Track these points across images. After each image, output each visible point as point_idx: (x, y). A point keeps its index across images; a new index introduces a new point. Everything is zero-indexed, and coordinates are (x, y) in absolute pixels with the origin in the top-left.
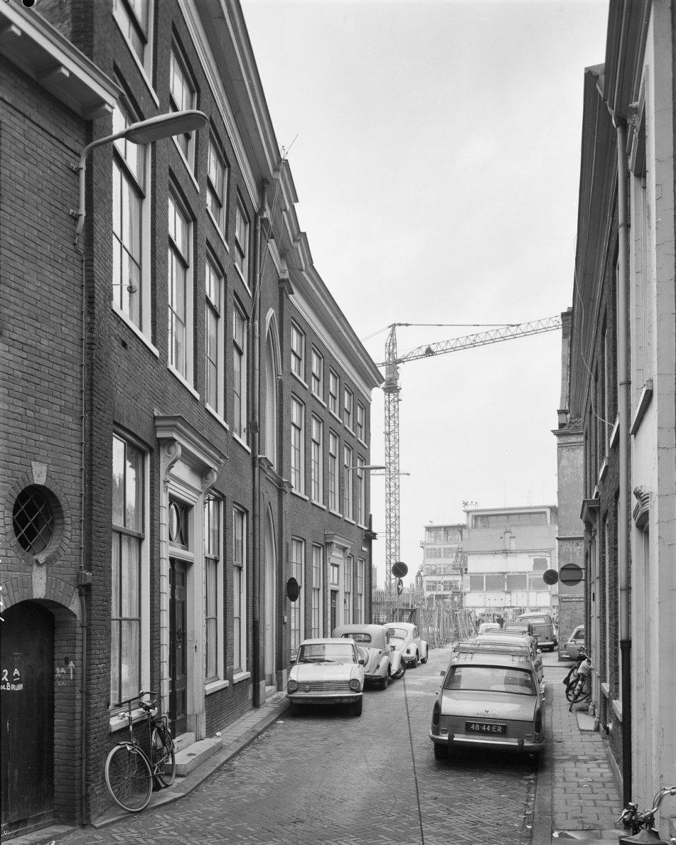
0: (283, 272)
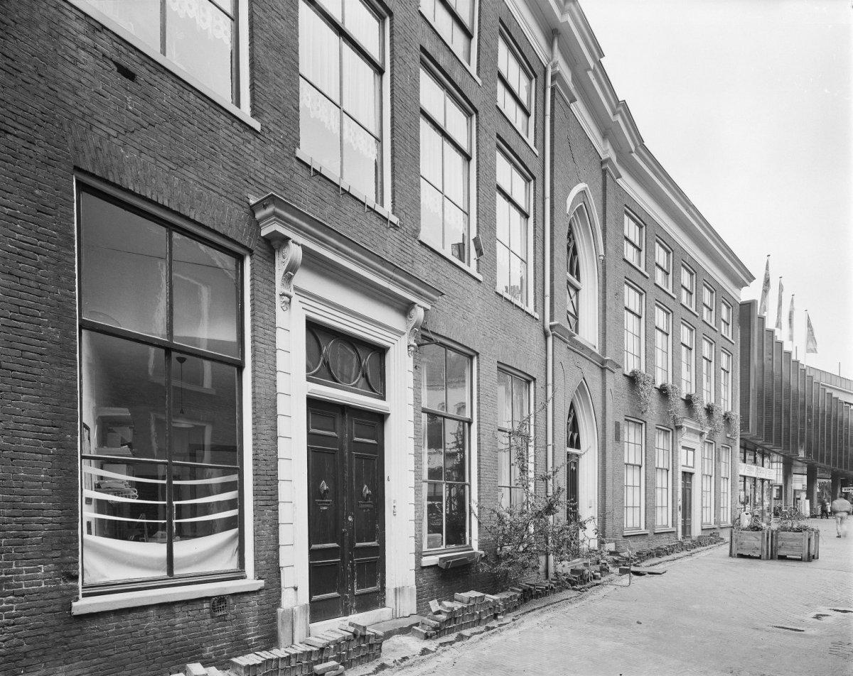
0: (605, 152)
